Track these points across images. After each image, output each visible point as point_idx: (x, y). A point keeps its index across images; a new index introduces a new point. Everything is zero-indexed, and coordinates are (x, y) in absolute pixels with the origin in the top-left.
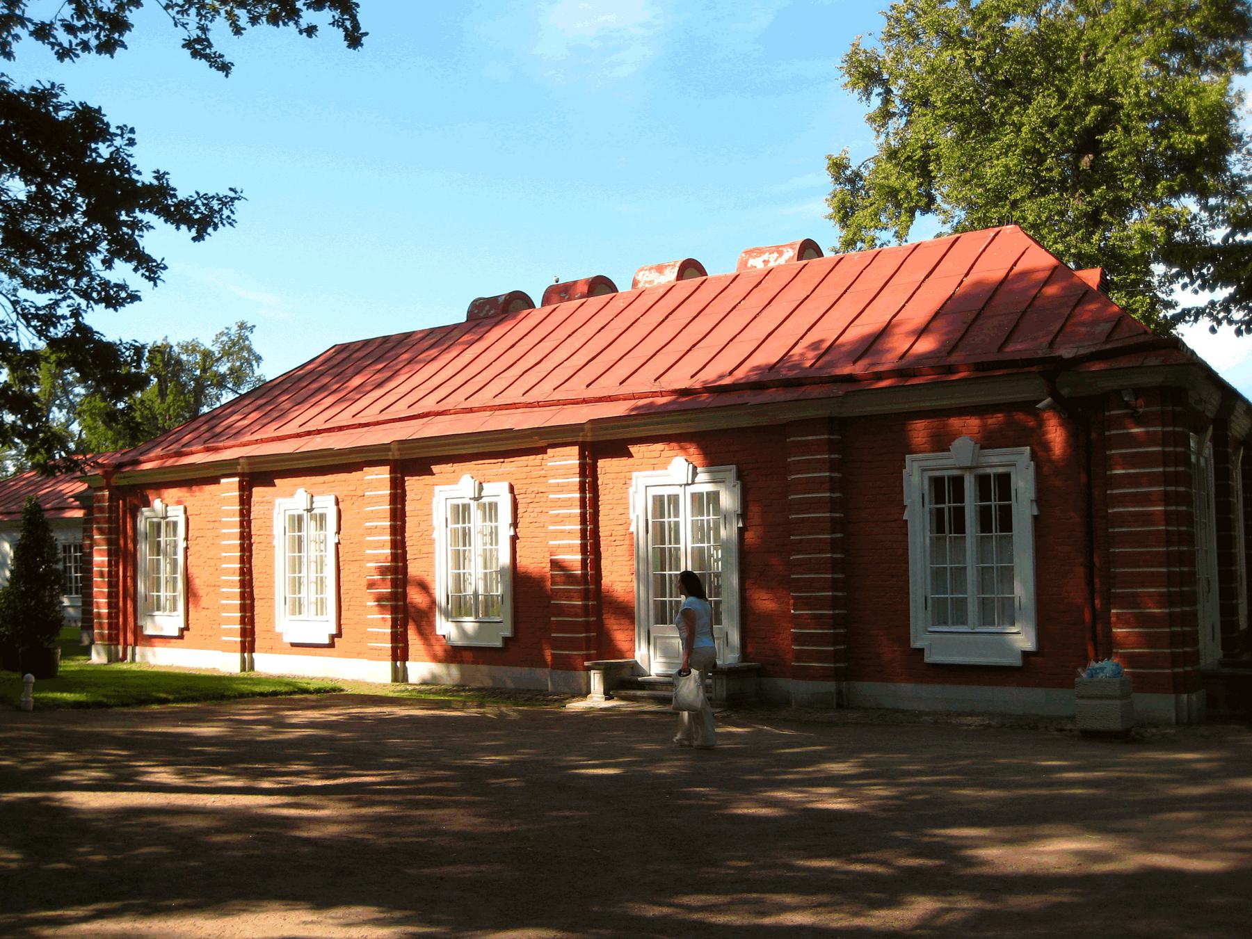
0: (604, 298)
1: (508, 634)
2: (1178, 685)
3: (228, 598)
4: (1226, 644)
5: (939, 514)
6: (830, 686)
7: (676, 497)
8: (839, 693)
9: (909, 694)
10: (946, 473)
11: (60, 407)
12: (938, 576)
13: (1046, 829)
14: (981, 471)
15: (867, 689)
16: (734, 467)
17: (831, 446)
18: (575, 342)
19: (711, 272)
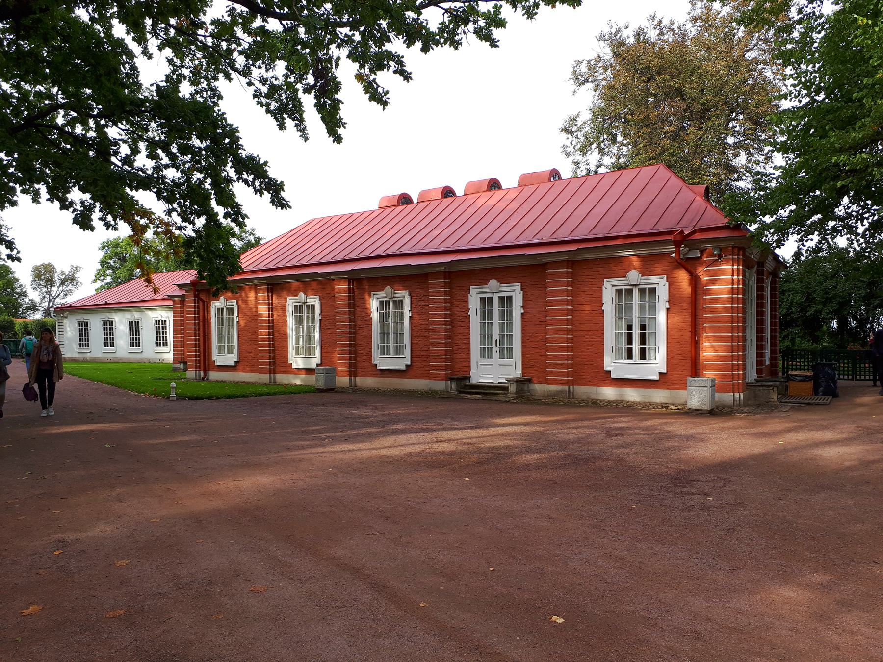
0: (451, 199)
1: (408, 363)
2: (734, 389)
3: (262, 347)
4: (759, 372)
5: (484, 312)
6: (566, 388)
7: (492, 298)
8: (569, 391)
9: (609, 393)
10: (624, 288)
11: (736, 155)
12: (483, 338)
13: (447, 423)
14: (641, 287)
15: (583, 391)
16: (665, 277)
17: (446, 285)
18: (447, 222)
19: (504, 186)
